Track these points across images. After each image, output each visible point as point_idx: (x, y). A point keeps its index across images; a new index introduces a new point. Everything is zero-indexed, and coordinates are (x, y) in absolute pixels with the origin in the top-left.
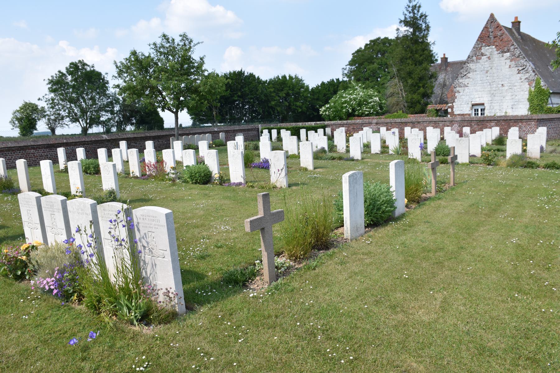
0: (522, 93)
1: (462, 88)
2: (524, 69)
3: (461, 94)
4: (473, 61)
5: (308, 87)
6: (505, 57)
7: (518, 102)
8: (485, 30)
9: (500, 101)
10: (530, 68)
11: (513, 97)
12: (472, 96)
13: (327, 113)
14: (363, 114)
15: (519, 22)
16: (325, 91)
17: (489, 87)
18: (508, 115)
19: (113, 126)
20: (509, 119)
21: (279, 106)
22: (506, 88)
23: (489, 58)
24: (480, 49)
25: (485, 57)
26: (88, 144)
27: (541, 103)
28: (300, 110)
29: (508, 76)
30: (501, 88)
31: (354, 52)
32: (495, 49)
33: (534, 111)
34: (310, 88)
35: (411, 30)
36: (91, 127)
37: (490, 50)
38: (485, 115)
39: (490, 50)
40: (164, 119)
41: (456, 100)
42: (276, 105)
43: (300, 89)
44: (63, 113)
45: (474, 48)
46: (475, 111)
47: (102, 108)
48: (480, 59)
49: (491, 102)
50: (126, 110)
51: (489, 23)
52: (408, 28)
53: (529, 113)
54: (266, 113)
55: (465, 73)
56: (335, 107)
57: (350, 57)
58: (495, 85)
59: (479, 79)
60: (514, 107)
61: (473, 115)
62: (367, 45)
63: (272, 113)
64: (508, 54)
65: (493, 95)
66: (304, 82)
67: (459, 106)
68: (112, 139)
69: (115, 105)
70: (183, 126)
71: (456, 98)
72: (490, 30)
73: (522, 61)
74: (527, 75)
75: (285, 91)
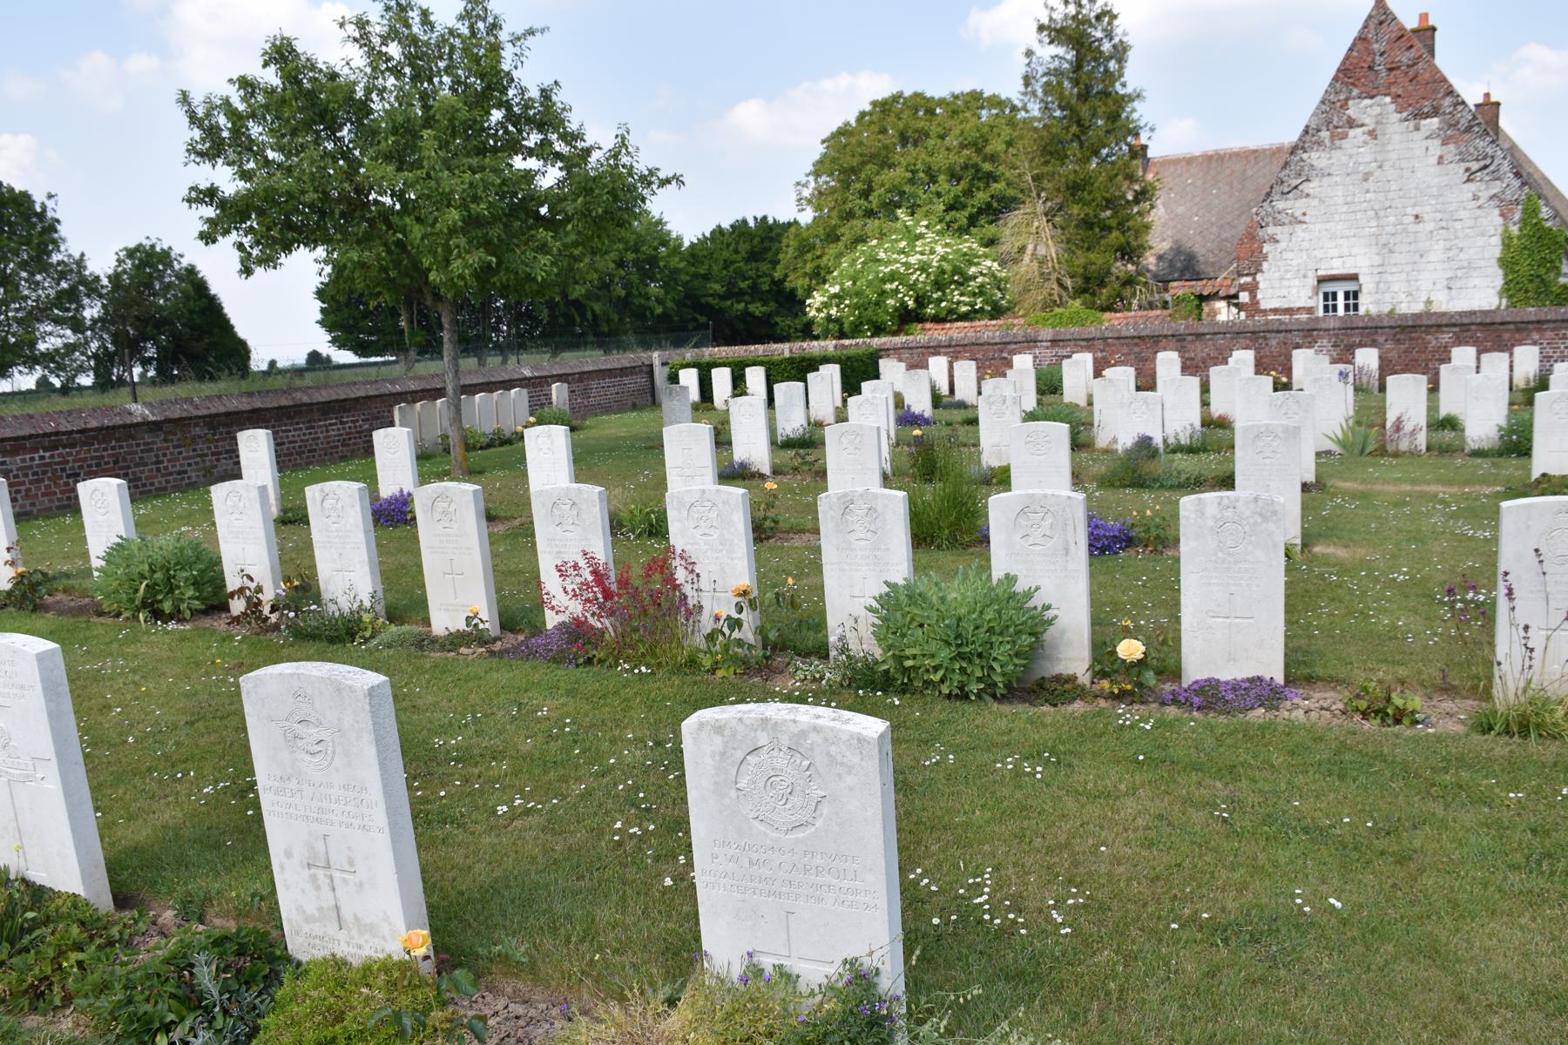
0: (1481, 241)
1: (1286, 229)
2: (1486, 167)
3: (1282, 245)
4: (1320, 143)
5: (679, 238)
6: (1424, 131)
7: (1469, 268)
8: (1360, 46)
9: (1409, 268)
10: (1506, 163)
11: (1451, 254)
12: (1318, 253)
13: (833, 311)
14: (951, 311)
15: (1434, 29)
16: (726, 254)
17: (1374, 223)
18: (1435, 308)
19: (82, 369)
20: (1498, 320)
21: (598, 299)
22: (1430, 226)
23: (1373, 134)
24: (1344, 106)
25: (1360, 130)
26: (73, 446)
27: (1542, 271)
28: (659, 310)
29: (1434, 191)
30: (1412, 228)
31: (826, 134)
32: (1393, 107)
33: (1521, 295)
34: (687, 244)
35: (1071, 55)
37: (1377, 110)
38: (1362, 311)
39: (1377, 110)
40: (250, 343)
41: (1265, 266)
42: (588, 296)
43: (656, 249)
45: (1323, 102)
46: (1326, 299)
48: (1344, 136)
49: (1381, 270)
50: (123, 318)
51: (1372, 26)
52: (1061, 51)
53: (1504, 302)
54: (561, 320)
55: (1295, 182)
56: (858, 294)
57: (818, 150)
58: (1392, 219)
59: (1340, 200)
60: (1455, 284)
61: (1321, 313)
62: (863, 114)
63: (578, 320)
64: (1434, 122)
65: (1387, 249)
66: (668, 227)
67: (1276, 283)
68: (169, 421)
69: (86, 301)
70: (280, 365)
71: (1265, 258)
72: (1376, 46)
73: (1481, 144)
74: (1497, 187)
75: (614, 255)
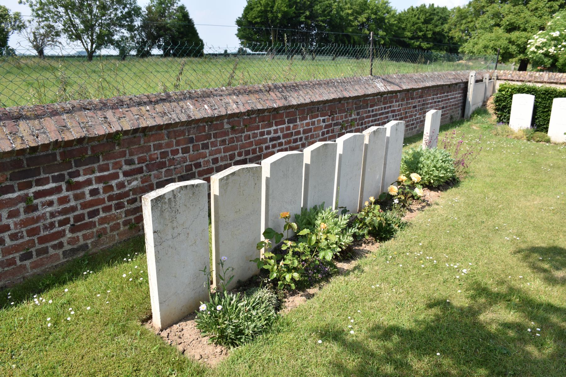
36: (98, 47)
40: (204, 42)
44: (59, 26)
47: (118, 22)
75: (366, 15)
